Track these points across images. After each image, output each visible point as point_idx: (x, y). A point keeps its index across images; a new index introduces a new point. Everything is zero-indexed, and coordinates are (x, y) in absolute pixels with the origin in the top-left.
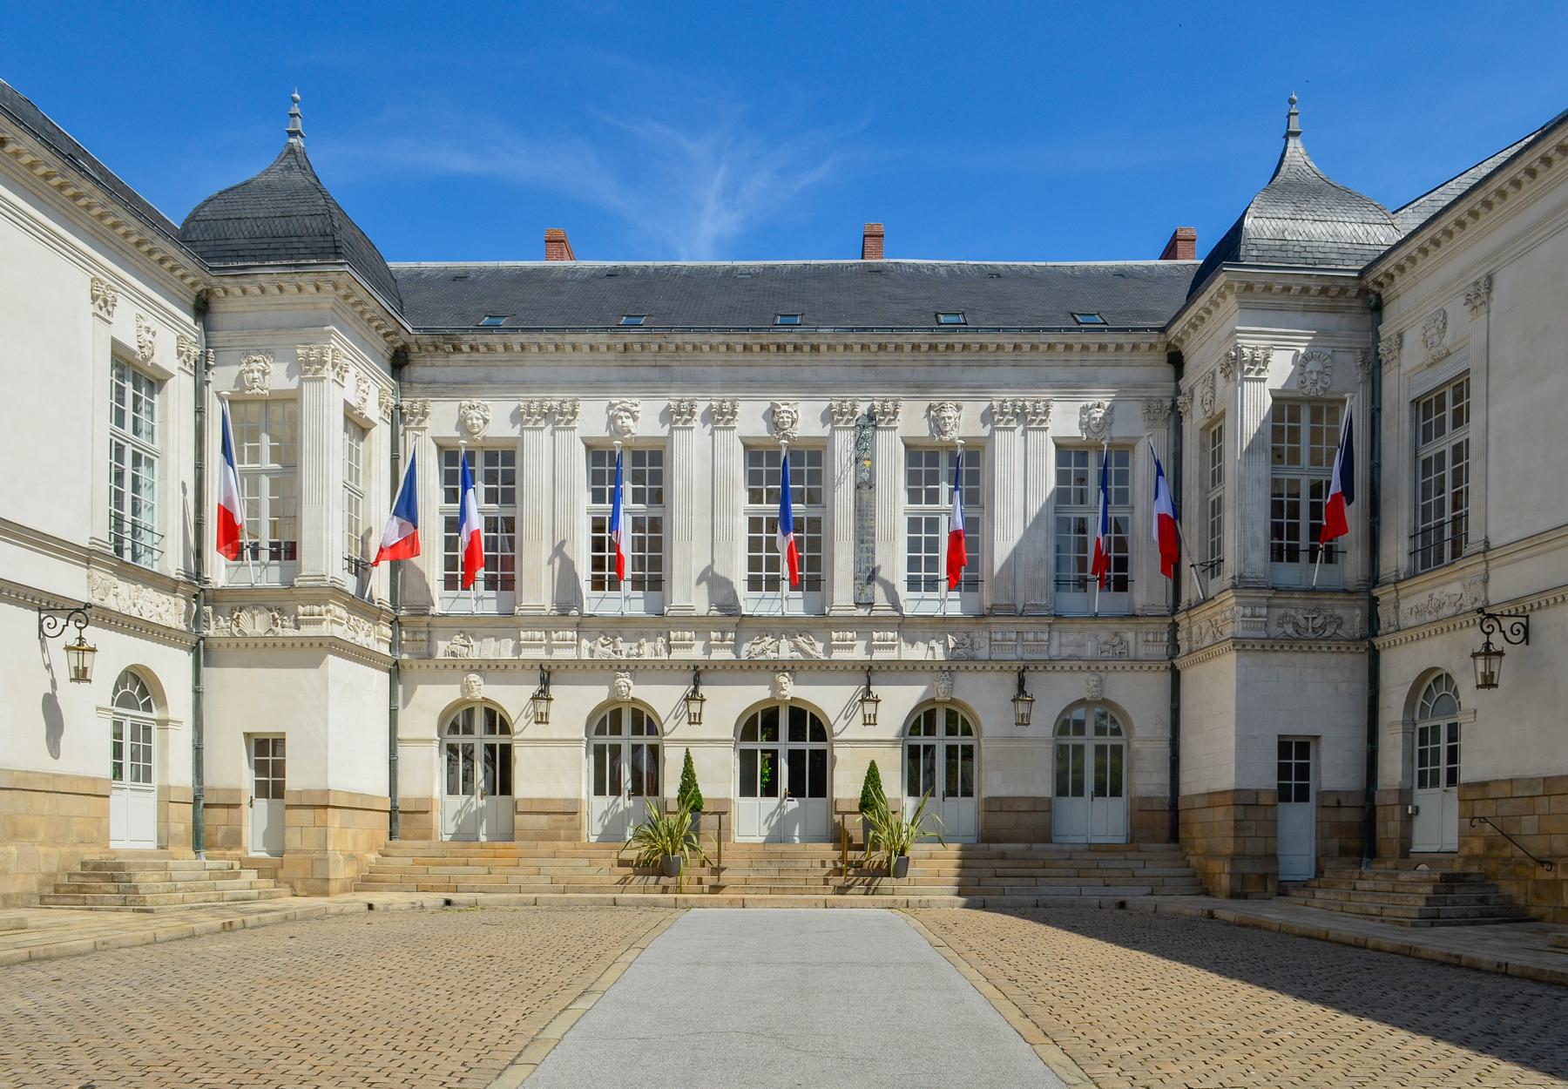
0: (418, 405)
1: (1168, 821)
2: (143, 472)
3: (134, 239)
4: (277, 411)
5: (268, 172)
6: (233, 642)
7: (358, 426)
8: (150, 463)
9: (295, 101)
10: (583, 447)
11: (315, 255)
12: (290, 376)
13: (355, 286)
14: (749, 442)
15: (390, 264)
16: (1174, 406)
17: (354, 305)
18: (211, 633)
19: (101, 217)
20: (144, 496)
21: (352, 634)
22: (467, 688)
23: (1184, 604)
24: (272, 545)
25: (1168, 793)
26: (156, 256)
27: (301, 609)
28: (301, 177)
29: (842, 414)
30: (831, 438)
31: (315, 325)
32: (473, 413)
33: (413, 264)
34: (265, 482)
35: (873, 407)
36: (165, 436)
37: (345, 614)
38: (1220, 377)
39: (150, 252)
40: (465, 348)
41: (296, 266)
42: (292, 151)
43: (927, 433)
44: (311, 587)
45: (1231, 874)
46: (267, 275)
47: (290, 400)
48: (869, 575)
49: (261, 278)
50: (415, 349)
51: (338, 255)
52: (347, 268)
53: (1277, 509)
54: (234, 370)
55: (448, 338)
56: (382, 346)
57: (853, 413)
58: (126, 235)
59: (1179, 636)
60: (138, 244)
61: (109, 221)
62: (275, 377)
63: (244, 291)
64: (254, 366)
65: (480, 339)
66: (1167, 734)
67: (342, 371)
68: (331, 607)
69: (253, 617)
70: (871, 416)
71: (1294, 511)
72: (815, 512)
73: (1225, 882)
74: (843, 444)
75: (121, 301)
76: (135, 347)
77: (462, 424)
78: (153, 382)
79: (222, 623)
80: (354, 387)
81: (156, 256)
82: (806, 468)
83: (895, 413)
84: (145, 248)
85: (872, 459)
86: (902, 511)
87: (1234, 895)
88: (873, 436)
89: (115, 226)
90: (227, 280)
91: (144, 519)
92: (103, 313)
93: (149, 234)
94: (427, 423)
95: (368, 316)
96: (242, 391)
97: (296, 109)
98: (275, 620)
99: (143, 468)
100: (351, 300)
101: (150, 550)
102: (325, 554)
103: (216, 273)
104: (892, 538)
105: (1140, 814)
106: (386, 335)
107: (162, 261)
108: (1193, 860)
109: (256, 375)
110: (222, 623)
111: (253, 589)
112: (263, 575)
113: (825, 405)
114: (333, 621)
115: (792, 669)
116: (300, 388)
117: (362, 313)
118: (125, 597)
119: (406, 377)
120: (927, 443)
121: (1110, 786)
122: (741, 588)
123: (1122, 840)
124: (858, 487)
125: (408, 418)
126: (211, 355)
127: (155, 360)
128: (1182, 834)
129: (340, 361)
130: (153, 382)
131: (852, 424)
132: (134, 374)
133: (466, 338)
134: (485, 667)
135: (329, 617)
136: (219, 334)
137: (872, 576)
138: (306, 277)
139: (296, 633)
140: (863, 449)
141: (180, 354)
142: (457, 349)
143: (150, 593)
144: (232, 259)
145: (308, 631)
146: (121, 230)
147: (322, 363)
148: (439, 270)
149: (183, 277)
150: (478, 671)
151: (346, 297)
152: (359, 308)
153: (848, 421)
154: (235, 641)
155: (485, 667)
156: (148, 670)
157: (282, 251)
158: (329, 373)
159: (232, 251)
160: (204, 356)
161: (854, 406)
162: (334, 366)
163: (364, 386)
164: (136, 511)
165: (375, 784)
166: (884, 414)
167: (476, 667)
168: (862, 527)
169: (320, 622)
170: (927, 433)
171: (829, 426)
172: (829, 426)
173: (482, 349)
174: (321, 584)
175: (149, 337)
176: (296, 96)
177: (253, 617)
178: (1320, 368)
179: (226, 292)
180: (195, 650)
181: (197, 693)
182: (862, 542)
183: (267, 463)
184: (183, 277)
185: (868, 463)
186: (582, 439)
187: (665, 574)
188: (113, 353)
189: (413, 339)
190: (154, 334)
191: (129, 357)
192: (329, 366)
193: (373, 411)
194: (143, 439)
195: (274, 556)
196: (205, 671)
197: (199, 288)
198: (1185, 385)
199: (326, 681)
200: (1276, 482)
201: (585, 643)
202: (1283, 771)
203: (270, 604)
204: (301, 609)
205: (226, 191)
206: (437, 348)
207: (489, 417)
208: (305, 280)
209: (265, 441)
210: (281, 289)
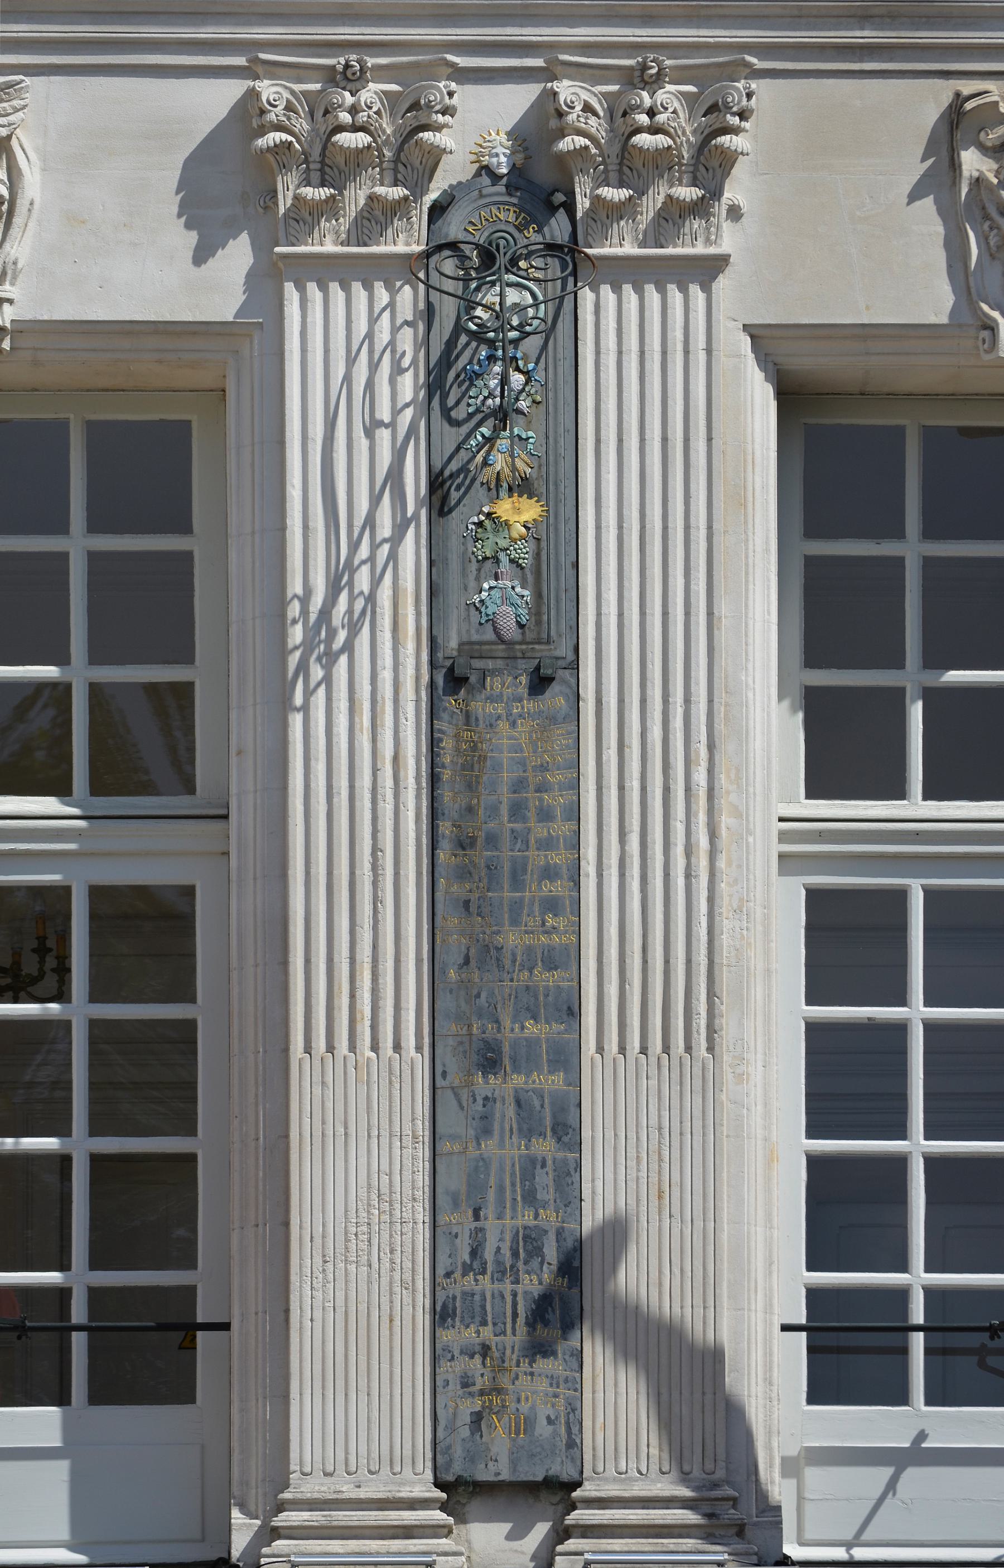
29: (331, 168)
30: (257, 331)
35: (545, 122)
43: (934, 302)
48: (533, 1287)
57: (410, 159)
70: (536, 182)
72: (147, 854)
74: (345, 370)
82: (77, 545)
83: (710, 165)
85: (553, 482)
86: (764, 847)
88: (561, 319)
104: (692, 1033)
113: (213, 100)
120: (925, 372)
122: (770, 1376)
124: (451, 679)
125: (290, 189)
131: (405, 241)
137: (566, 1295)
140: (488, 413)
153: (378, 216)
161: (416, 115)
166: (628, 165)
168: (485, 955)
170: (934, 302)
171: (238, 256)
172: (238, 256)
182: (490, 1060)
185: (520, 513)
186: (759, 336)
187: (215, 1278)
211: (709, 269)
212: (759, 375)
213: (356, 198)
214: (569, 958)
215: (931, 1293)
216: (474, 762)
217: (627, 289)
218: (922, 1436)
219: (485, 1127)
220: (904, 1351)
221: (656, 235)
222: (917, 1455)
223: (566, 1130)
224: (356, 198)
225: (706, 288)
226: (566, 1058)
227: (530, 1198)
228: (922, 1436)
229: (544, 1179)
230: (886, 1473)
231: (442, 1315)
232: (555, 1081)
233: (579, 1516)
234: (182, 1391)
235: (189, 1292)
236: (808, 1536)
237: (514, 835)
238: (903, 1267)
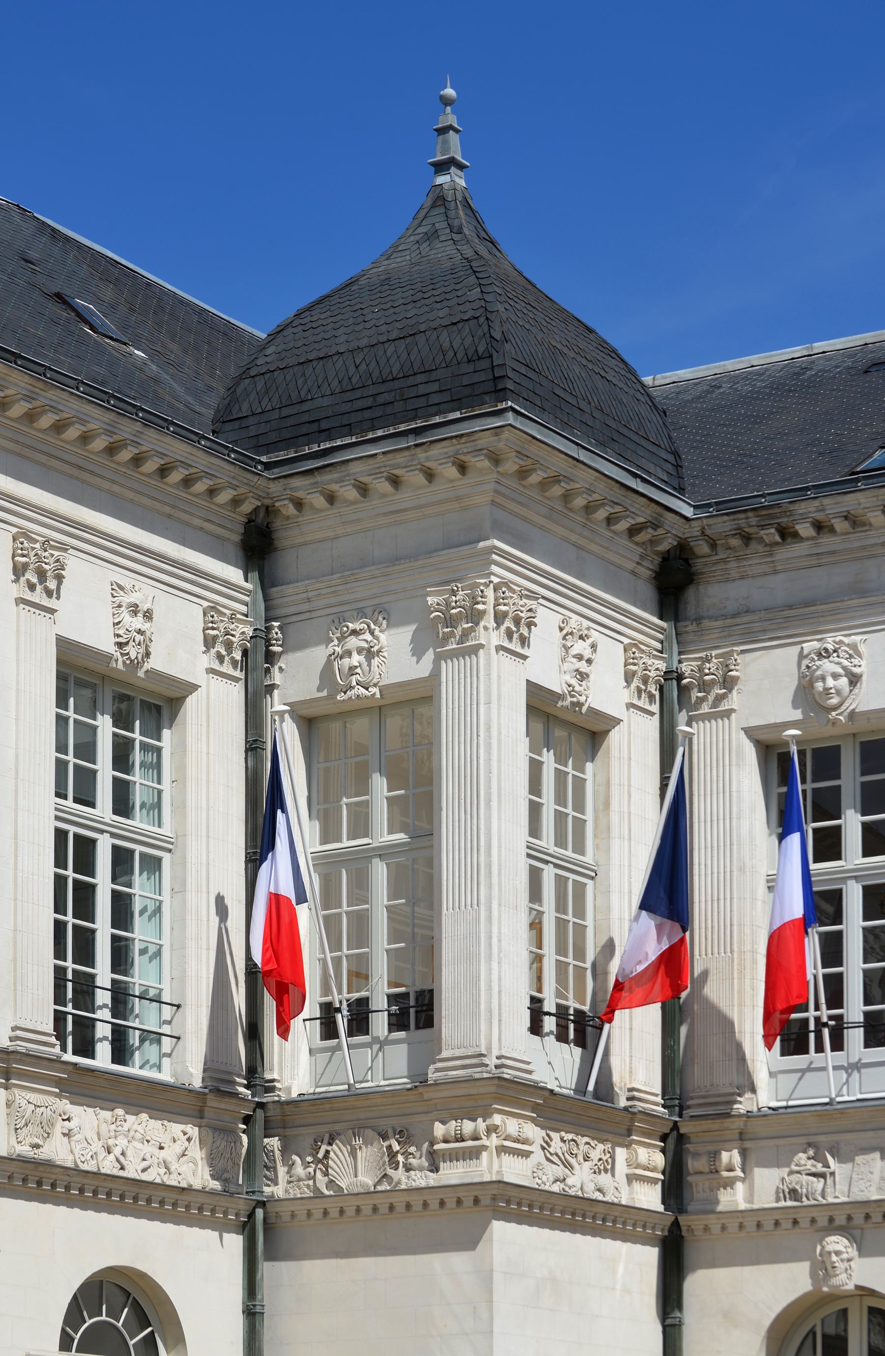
0: (712, 666)
2: (140, 888)
3: (99, 444)
4: (394, 724)
5: (394, 250)
6: (317, 1208)
7: (565, 728)
8: (153, 865)
9: (447, 101)
10: (750, 753)
11: (457, 403)
12: (418, 652)
13: (534, 449)
14: (764, 737)
15: (648, 380)
17: (544, 485)
18: (278, 1191)
19: (31, 417)
20: (141, 932)
21: (560, 1171)
22: (822, 1268)
24: (392, 999)
26: (151, 466)
27: (439, 1130)
28: (450, 249)
31: (456, 548)
32: (828, 666)
33: (797, 351)
34: (380, 872)
36: (180, 807)
37: (533, 1132)
39: (137, 461)
40: (805, 529)
41: (416, 432)
42: (439, 199)
44: (456, 1082)
46: (366, 460)
47: (417, 702)
49: (356, 468)
50: (703, 548)
51: (500, 393)
52: (510, 418)
54: (318, 655)
55: (766, 513)
56: (628, 555)
58: (85, 439)
60: (111, 450)
61: (46, 421)
62: (392, 656)
63: (331, 498)
64: (353, 642)
65: (832, 506)
67: (519, 630)
68: (497, 1119)
69: (353, 1154)
75: (76, 567)
76: (107, 645)
77: (807, 693)
78: (150, 705)
79: (299, 1170)
80: (556, 651)
81: (151, 466)
84: (125, 455)
89: (59, 427)
90: (296, 482)
91: (141, 977)
92: (38, 597)
93: (128, 428)
94: (735, 700)
95: (579, 502)
96: (331, 697)
97: (450, 118)
98: (392, 1155)
99: (138, 879)
100: (534, 478)
101: (151, 1037)
102: (492, 1006)
103: (277, 472)
106: (632, 532)
107: (163, 471)
109: (356, 659)
110: (299, 1170)
111: (353, 1096)
112: (380, 1064)
114: (502, 1150)
116: (435, 674)
117: (567, 497)
118: (86, 1137)
119: (691, 610)
125: (695, 694)
126: (276, 633)
127: (156, 663)
129: (514, 604)
130: (150, 705)
132: (113, 701)
133: (802, 508)
134: (859, 1219)
135: (494, 1141)
136: (288, 589)
138: (437, 451)
139: (432, 1179)
141: (209, 642)
142: (787, 534)
143: (143, 1124)
144: (309, 437)
145: (453, 1173)
146: (73, 433)
147: (476, 617)
148: (846, 353)
149: (212, 492)
150: (846, 1230)
151: (523, 474)
152: (557, 491)
154: (319, 1205)
155: (859, 1219)
156: (143, 1276)
157: (398, 406)
158: (490, 636)
159: (291, 428)
160: (263, 636)
162: (499, 618)
163: (580, 647)
164: (121, 957)
167: (840, 1220)
169: (474, 1154)
171: (429, 656)
173: (840, 525)
174: (476, 1073)
175: (138, 622)
176: (450, 92)
177: (353, 1154)
179: (299, 504)
180: (247, 1228)
181: (252, 1315)
183: (383, 835)
184: (212, 492)
188: (59, 662)
189: (696, 528)
190: (148, 615)
191: (100, 669)
192: (489, 621)
193: (607, 690)
194: (139, 822)
195: (398, 1022)
196: (267, 1269)
197: (247, 507)
199: (486, 1278)
201: (621, 1154)
203: (386, 1124)
204: (439, 1130)
205: (310, 308)
206: (747, 539)
207: (863, 667)
208: (436, 456)
209: (380, 785)
210: (395, 482)
211: (728, 714)
212: (747, 741)
213: (458, 632)
217: (707, 722)
218: (811, 1063)
220: (65, 987)
221: (714, 706)
222: (809, 1069)
224: (458, 632)
225: (729, 719)
228: (811, 1063)
230: (800, 1074)
236: (779, 1098)
237: (144, 747)
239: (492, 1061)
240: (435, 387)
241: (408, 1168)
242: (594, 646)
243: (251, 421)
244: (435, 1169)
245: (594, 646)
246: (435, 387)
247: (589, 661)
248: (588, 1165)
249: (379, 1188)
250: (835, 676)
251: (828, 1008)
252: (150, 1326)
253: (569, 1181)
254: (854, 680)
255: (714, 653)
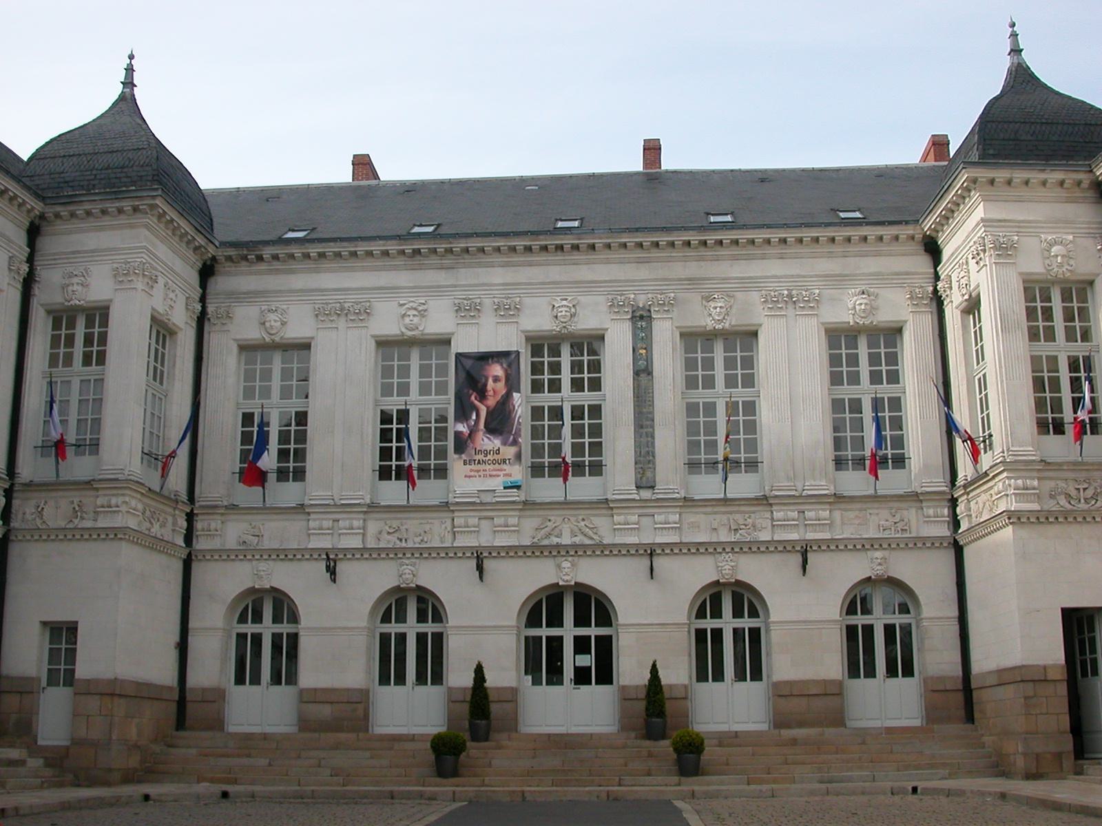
1: (963, 698)
16: (935, 291)
23: (960, 481)
25: (959, 672)
32: (272, 316)
38: (972, 262)
45: (1025, 754)
48: (645, 458)
53: (1038, 384)
59: (958, 510)
66: (955, 612)
71: (1055, 385)
73: (1020, 762)
87: (1030, 776)
105: (934, 691)
108: (987, 739)
115: (576, 551)
121: (902, 665)
123: (917, 723)
128: (976, 715)
156: (250, 486)
163: (172, 295)
165: (162, 672)
174: (119, 476)
178: (1064, 252)
182: (642, 427)
198: (943, 271)
200: (1035, 361)
202: (54, 655)
214: (652, 413)
215: (435, 464)
216: (639, 386)
219: (641, 437)
220: (544, 470)
223: (653, 437)
226: (653, 427)
227: (648, 447)
229: (650, 443)
231: (636, 463)
232: (651, 430)
233: (656, 491)
234: (904, 467)
235: (904, 454)
238: (584, 443)
239: (126, 473)
240: (124, 175)
241: (82, 518)
242: (176, 295)
243: (35, 178)
244: (95, 520)
245: (176, 295)
246: (124, 175)
247: (175, 302)
248: (158, 523)
249: (67, 527)
250: (275, 321)
251: (846, 349)
252: (841, 336)
253: (152, 530)
254: (284, 324)
255: (223, 305)
